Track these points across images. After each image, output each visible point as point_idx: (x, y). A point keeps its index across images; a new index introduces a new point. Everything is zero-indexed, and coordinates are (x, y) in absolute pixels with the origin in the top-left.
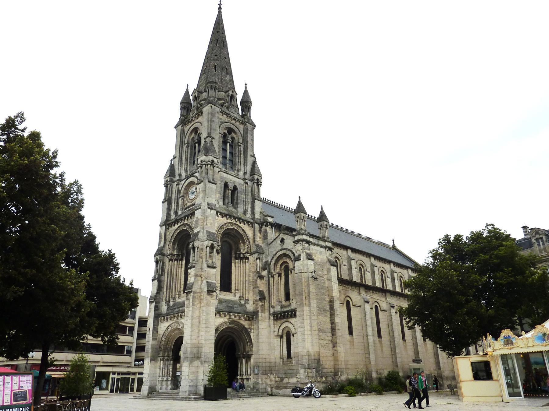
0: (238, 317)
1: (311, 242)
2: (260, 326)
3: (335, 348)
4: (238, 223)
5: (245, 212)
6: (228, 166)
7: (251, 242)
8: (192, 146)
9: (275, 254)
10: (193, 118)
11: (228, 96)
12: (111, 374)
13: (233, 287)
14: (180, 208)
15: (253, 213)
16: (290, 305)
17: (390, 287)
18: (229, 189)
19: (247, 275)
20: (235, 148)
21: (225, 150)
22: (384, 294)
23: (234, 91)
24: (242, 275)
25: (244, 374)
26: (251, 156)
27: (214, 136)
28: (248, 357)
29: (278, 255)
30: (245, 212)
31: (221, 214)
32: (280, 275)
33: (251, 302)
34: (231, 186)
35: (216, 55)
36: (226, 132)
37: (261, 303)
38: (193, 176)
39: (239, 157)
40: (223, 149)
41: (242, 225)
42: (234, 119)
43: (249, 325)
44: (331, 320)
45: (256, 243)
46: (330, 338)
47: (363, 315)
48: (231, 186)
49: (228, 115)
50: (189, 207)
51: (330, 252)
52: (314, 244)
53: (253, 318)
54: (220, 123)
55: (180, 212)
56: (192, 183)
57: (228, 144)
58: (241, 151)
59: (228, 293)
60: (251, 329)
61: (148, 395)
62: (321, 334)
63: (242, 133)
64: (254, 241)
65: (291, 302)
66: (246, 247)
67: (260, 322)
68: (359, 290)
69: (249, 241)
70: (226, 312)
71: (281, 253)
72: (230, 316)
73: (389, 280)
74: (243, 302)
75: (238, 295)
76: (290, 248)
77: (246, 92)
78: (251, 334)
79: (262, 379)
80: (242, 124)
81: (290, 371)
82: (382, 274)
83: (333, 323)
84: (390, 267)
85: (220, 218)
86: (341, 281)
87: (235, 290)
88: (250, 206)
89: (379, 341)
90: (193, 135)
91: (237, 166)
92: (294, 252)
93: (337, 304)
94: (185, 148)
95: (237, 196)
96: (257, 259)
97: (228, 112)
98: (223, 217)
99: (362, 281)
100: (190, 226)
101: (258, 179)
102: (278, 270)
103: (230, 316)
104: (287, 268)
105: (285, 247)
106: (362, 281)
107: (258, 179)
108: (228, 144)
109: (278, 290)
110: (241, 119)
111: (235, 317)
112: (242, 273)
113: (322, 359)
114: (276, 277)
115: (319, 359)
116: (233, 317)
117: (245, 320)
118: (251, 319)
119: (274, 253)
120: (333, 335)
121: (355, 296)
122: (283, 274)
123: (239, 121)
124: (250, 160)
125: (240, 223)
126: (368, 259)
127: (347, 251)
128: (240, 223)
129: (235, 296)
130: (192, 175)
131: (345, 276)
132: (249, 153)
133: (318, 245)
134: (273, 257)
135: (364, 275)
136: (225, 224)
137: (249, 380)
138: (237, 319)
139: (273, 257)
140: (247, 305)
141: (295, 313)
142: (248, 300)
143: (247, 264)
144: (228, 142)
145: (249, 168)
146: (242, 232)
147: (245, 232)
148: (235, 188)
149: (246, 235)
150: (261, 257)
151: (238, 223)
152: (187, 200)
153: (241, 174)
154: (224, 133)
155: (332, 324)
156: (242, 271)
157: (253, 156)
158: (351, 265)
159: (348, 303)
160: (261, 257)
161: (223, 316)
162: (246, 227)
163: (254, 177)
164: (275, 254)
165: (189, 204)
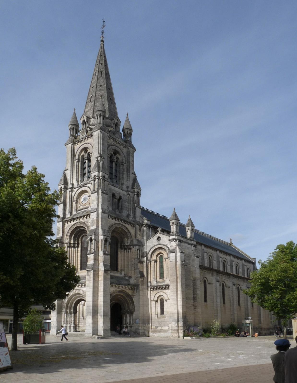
0: (124, 288)
1: (182, 241)
2: (141, 294)
3: (196, 310)
4: (124, 224)
5: (128, 216)
6: (115, 181)
7: (133, 237)
8: (82, 162)
9: (153, 247)
10: (83, 139)
11: (114, 124)
12: (9, 321)
13: (119, 268)
14: (74, 209)
15: (134, 217)
16: (164, 282)
17: (229, 271)
18: (115, 198)
19: (130, 260)
20: (119, 166)
21: (111, 168)
22: (228, 276)
23: (118, 120)
24: (126, 260)
25: (128, 323)
26: (132, 173)
27: (104, 157)
28: (131, 313)
29: (155, 248)
30: (128, 216)
31: (111, 217)
32: (156, 261)
33: (133, 278)
34: (117, 196)
35: (101, 86)
36: (112, 153)
37: (141, 279)
38: (86, 186)
39: (123, 174)
40: (110, 167)
41: (126, 225)
42: (119, 143)
43: (132, 293)
44: (193, 292)
45: (137, 238)
46: (192, 303)
47: (214, 289)
48: (117, 196)
49: (114, 140)
50: (82, 209)
51: (195, 248)
52: (184, 242)
53: (135, 289)
54: (108, 146)
55: (74, 213)
56: (85, 192)
57: (114, 163)
58: (124, 169)
59: (116, 272)
60: (133, 296)
61: (57, 335)
62: (187, 300)
63: (125, 155)
64: (136, 237)
65: (165, 279)
66: (129, 241)
67: (140, 292)
68: (213, 273)
69: (131, 237)
70: (117, 284)
71: (157, 247)
72: (119, 287)
73: (228, 267)
74: (127, 278)
75: (123, 273)
76: (165, 244)
77: (128, 121)
78: (134, 299)
79: (142, 327)
80: (125, 147)
81: (163, 323)
82: (224, 263)
83: (194, 293)
84: (242, 262)
85: (111, 220)
86: (202, 267)
87: (121, 270)
88: (131, 212)
89: (224, 306)
90: (83, 153)
91: (121, 181)
92: (169, 247)
93: (198, 282)
94: (75, 162)
95: (122, 204)
96: (138, 250)
97: (114, 137)
98: (112, 219)
99: (210, 266)
100: (86, 224)
101: (138, 192)
102: (154, 257)
103: (119, 287)
104: (161, 258)
105: (161, 243)
106: (210, 266)
107: (138, 192)
108: (114, 163)
109: (155, 272)
110: (124, 143)
111: (123, 287)
112: (126, 259)
113: (187, 315)
114: (153, 262)
115: (186, 316)
116: (121, 287)
117: (130, 290)
118: (133, 289)
119: (152, 246)
120: (194, 301)
121: (212, 278)
122: (158, 261)
123: (123, 145)
124: (132, 176)
125: (125, 224)
126: (215, 252)
127: (217, 252)
128: (125, 224)
129: (121, 274)
130: (84, 185)
131: (206, 265)
132: (131, 171)
133: (187, 243)
134: (151, 249)
135: (212, 262)
136: (114, 224)
137: (132, 327)
138: (124, 289)
139: (151, 249)
140: (130, 280)
141: (169, 287)
142: (131, 277)
143: (130, 252)
144: (113, 162)
145: (130, 183)
146: (126, 231)
147: (128, 230)
148: (120, 198)
149: (129, 232)
150: (141, 248)
151: (124, 224)
152: (80, 204)
153: (124, 187)
154: (111, 154)
155: (194, 294)
156: (126, 257)
157: (134, 173)
158: (204, 256)
159: (205, 282)
160: (141, 248)
161: (114, 286)
162: (129, 227)
163: (135, 188)
164: (153, 247)
165: (81, 207)
